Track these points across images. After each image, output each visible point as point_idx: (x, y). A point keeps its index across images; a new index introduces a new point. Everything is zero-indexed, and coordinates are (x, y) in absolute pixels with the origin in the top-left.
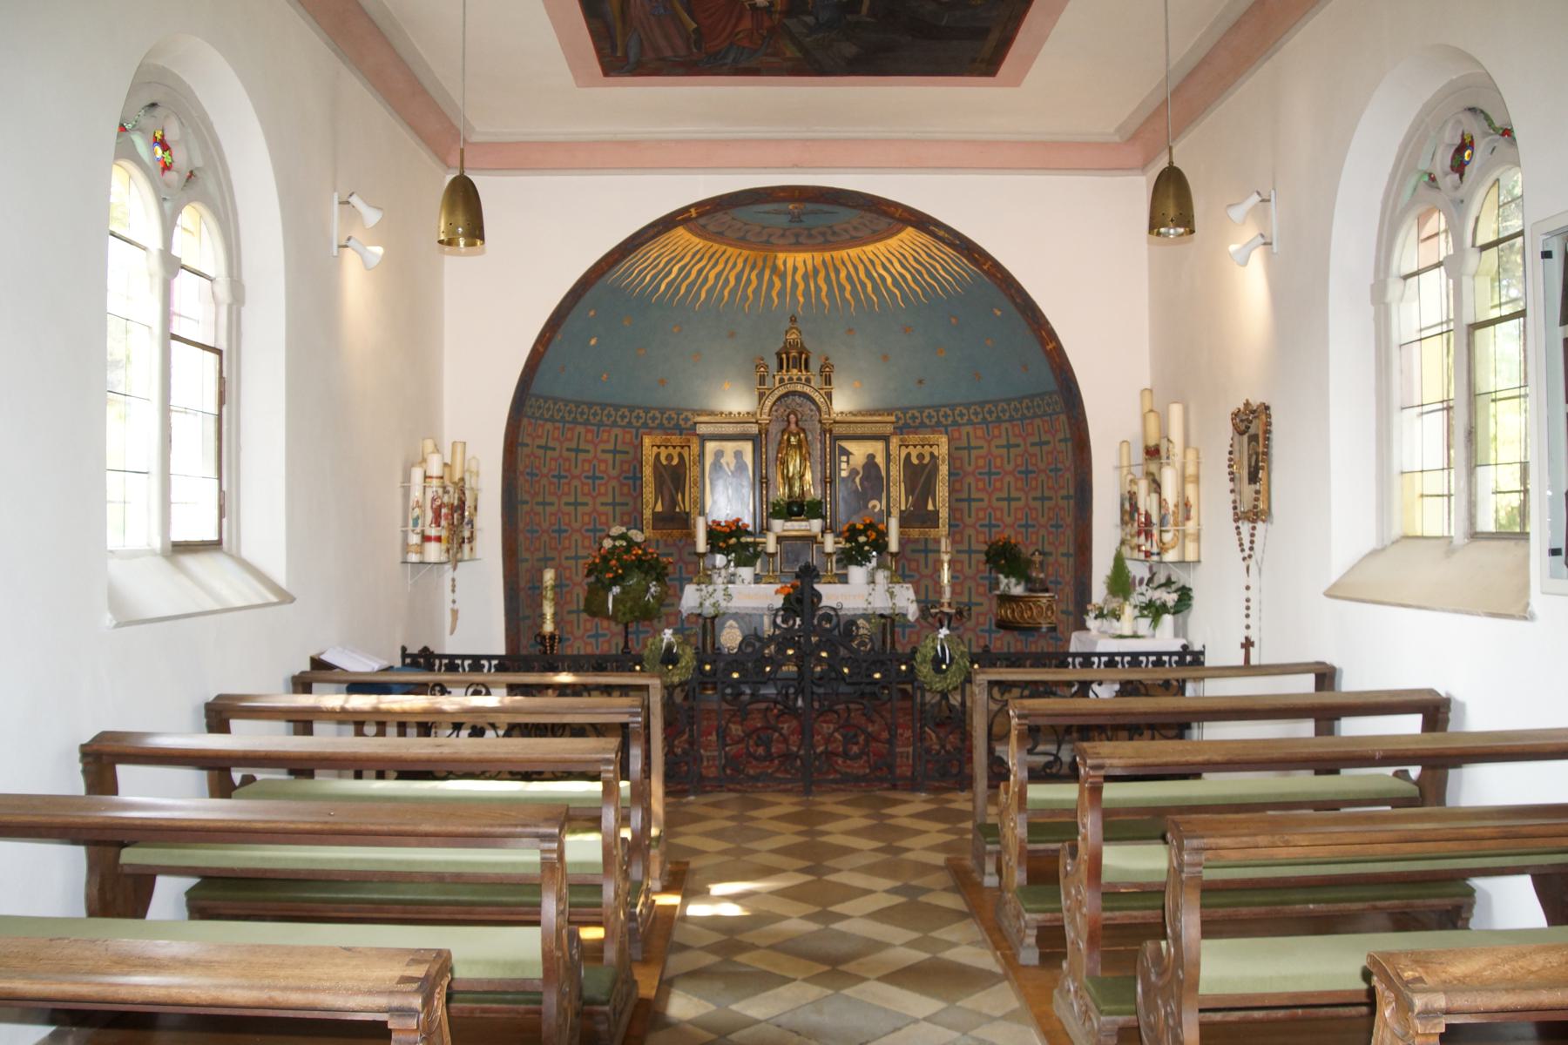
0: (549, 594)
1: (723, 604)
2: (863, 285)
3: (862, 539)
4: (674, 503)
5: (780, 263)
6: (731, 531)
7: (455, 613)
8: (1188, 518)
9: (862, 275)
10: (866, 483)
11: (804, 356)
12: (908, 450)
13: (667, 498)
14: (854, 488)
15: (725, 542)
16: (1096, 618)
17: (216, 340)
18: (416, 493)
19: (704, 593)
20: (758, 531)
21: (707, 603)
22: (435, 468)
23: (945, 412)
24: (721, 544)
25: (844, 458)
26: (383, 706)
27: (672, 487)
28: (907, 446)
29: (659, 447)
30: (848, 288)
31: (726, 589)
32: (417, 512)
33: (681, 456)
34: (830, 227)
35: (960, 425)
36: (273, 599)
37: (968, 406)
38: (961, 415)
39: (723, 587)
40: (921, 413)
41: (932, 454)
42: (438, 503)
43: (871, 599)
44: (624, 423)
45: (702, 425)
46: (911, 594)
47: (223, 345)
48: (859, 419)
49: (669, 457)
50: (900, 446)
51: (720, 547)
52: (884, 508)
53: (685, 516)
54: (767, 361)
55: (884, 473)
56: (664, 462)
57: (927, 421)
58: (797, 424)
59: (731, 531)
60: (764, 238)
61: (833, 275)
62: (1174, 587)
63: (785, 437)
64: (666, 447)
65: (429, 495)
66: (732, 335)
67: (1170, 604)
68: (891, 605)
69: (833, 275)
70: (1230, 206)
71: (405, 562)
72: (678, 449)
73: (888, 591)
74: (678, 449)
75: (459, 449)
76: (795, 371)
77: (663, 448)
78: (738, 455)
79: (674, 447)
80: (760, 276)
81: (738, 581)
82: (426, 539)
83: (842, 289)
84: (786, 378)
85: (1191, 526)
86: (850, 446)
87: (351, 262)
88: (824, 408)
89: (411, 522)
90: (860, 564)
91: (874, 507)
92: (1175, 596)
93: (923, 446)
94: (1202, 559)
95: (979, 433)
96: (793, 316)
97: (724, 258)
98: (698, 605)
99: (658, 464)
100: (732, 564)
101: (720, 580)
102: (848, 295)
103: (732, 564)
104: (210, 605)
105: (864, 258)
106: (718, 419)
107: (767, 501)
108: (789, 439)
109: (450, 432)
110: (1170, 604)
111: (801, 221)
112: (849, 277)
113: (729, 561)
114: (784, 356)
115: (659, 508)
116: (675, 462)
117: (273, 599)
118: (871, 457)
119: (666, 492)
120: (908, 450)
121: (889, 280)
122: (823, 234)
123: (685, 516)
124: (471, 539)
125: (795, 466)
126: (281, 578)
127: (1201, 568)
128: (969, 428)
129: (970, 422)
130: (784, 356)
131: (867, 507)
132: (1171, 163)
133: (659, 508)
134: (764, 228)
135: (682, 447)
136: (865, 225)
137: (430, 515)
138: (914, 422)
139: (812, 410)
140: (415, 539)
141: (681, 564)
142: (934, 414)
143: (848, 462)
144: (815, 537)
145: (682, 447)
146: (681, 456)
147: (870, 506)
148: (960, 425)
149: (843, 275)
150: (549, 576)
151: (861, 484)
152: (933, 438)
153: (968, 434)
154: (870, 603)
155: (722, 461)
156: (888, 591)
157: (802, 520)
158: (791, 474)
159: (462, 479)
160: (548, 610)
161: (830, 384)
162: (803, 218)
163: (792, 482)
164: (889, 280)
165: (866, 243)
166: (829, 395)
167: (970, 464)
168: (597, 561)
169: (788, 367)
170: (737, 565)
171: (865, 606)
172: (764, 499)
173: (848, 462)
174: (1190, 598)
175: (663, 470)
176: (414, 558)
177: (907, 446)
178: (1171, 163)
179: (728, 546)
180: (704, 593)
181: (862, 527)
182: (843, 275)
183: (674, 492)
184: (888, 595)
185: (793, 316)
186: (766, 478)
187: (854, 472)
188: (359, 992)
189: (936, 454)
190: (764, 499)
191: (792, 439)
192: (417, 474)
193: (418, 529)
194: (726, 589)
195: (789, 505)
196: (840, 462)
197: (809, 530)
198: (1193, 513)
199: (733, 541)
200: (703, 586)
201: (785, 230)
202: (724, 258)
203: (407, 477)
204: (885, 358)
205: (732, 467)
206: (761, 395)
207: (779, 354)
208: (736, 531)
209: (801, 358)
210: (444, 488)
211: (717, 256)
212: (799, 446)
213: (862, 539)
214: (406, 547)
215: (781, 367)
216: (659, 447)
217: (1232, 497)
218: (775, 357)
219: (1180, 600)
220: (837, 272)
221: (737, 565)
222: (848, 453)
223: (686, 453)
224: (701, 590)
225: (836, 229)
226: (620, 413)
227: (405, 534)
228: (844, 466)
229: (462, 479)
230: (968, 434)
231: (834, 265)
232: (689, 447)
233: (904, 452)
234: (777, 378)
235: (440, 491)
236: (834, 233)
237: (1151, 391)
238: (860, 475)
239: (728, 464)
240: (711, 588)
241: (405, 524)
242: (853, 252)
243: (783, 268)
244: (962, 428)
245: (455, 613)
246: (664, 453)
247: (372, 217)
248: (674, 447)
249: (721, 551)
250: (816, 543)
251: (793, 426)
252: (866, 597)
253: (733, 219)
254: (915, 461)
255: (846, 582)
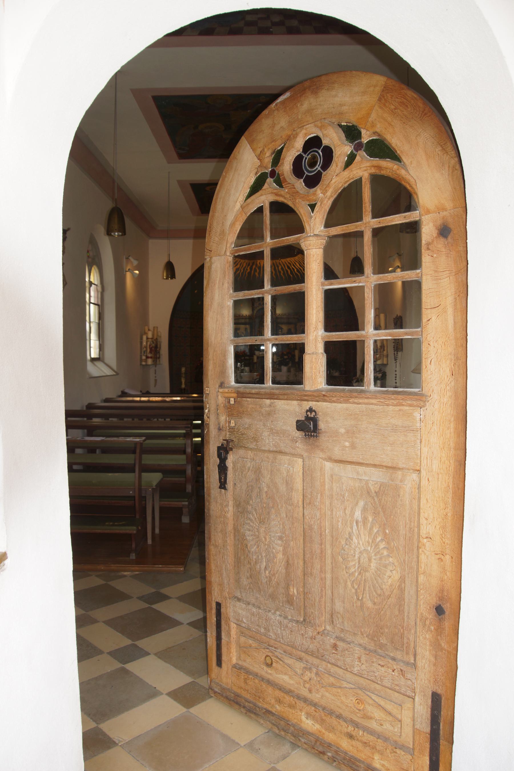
0: (183, 375)
2: (287, 271)
5: (258, 263)
7: (156, 380)
8: (384, 350)
9: (287, 268)
16: (356, 382)
17: (98, 302)
18: (144, 343)
22: (150, 335)
25: (280, 330)
26: (151, 400)
30: (282, 272)
32: (145, 349)
36: (115, 374)
42: (151, 346)
47: (100, 303)
61: (277, 268)
62: (382, 372)
65: (148, 344)
67: (379, 377)
69: (277, 268)
70: (390, 257)
71: (141, 365)
75: (156, 329)
78: (246, 329)
80: (251, 269)
81: (244, 371)
82: (147, 357)
83: (280, 272)
85: (385, 352)
87: (128, 275)
89: (143, 352)
92: (381, 375)
94: (389, 363)
97: (240, 263)
102: (282, 274)
104: (104, 375)
105: (287, 262)
109: (152, 323)
110: (379, 377)
112: (282, 268)
117: (115, 374)
121: (295, 270)
124: (159, 358)
126: (115, 368)
127: (388, 366)
132: (357, 255)
137: (148, 350)
140: (144, 358)
149: (280, 268)
150: (183, 370)
159: (157, 339)
160: (183, 381)
164: (295, 270)
165: (287, 257)
168: (199, 364)
170: (244, 366)
174: (386, 375)
176: (144, 363)
178: (357, 255)
182: (280, 268)
192: (145, 338)
193: (145, 354)
198: (385, 348)
199: (243, 358)
202: (240, 263)
203: (141, 338)
210: (153, 341)
211: (238, 262)
213: (285, 357)
214: (141, 360)
217: (394, 344)
219: (382, 376)
220: (278, 267)
221: (244, 366)
222: (282, 329)
227: (141, 356)
229: (157, 339)
231: (277, 265)
235: (152, 342)
237: (379, 309)
241: (141, 353)
242: (283, 260)
243: (259, 265)
245: (156, 380)
247: (135, 263)
255: (281, 371)
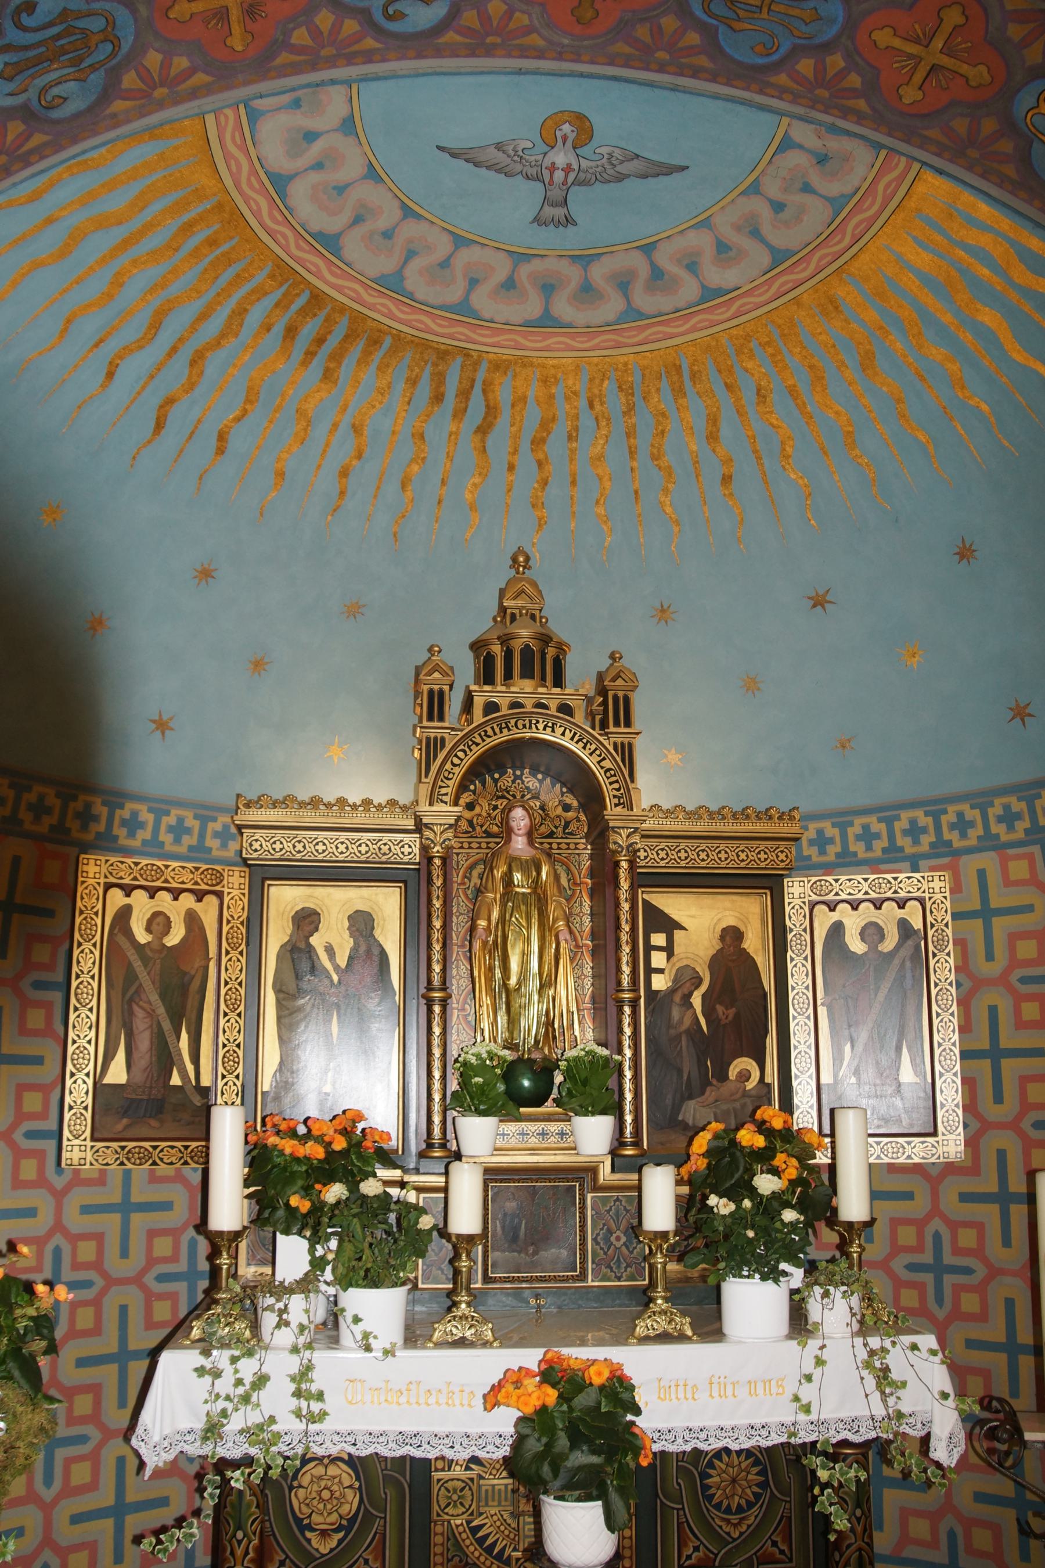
1: (288, 1424)
3: (766, 1184)
4: (166, 1059)
6: (330, 1154)
10: (720, 1009)
11: (551, 652)
12: (835, 916)
13: (144, 1042)
14: (687, 1022)
15: (307, 1191)
19: (225, 1385)
20: (413, 1148)
21: (235, 1423)
23: (913, 822)
24: (294, 1201)
25: (659, 939)
27: (161, 1010)
28: (832, 907)
29: (128, 891)
31: (305, 1373)
33: (192, 920)
34: (648, 249)
35: (957, 853)
37: (981, 799)
38: (962, 825)
39: (293, 1364)
40: (843, 827)
41: (904, 925)
43: (807, 1392)
44: (43, 828)
45: (259, 834)
46: (939, 1377)
48: (701, 827)
49: (159, 922)
50: (813, 906)
51: (292, 1211)
52: (772, 1076)
53: (197, 1101)
54: (448, 657)
55: (768, 983)
56: (142, 937)
57: (858, 848)
58: (530, 835)
59: (330, 1154)
60: (454, 294)
63: (498, 874)
64: (152, 893)
66: (354, 610)
68: (879, 1411)
72: (187, 901)
73: (868, 1365)
74: (187, 901)
76: (527, 685)
77: (139, 896)
79: (176, 894)
81: (348, 1334)
84: (504, 702)
86: (673, 904)
88: (608, 791)
90: (773, 1275)
91: (745, 1076)
93: (878, 905)
95: (1019, 869)
96: (520, 551)
98: (199, 1425)
99: (122, 940)
100: (328, 1275)
101: (285, 1337)
103: (328, 1275)
106: (309, 817)
107: (444, 1055)
108: (508, 881)
111: (569, 221)
113: (318, 1264)
114: (497, 649)
115: (117, 1074)
116: (175, 937)
118: (732, 936)
119: (141, 1022)
120: (835, 916)
122: (624, 283)
123: (197, 1101)
125: (525, 956)
128: (988, 861)
129: (989, 843)
130: (497, 649)
131: (723, 1077)
133: (117, 1074)
134: (460, 241)
135: (200, 896)
136: (755, 233)
138: (822, 852)
139: (567, 808)
141: (149, 1279)
142: (881, 828)
143: (669, 950)
144: (592, 1170)
145: (200, 896)
146: (192, 920)
147: (733, 1072)
148: (957, 853)
151: (708, 1010)
152: (908, 882)
153: (982, 874)
154: (807, 1409)
155: (316, 941)
156: (868, 1365)
157: (549, 1118)
158: (513, 981)
161: (628, 724)
162: (577, 194)
163: (516, 1003)
166: (627, 753)
167: (990, 956)
169: (508, 676)
170: (345, 1281)
171: (789, 1419)
172: (437, 1052)
173: (669, 950)
175: (137, 965)
177: (832, 907)
179: (318, 1207)
180: (225, 1385)
181: (760, 1142)
183: (167, 1025)
184: (871, 1382)
185: (520, 551)
186: (430, 1003)
187: (686, 979)
188: (444, 970)
189: (917, 924)
190: (437, 1052)
191: (517, 877)
194: (305, 1373)
195: (510, 1072)
196: (649, 948)
197: (501, 1121)
200: (221, 1357)
201: (520, 258)
204: (751, 685)
205: (342, 961)
206: (432, 747)
207: (477, 646)
208: (345, 1153)
209: (543, 655)
212: (539, 899)
213: (766, 1184)
215: (487, 678)
216: (128, 891)
218: (470, 655)
222: (669, 926)
223: (208, 911)
224: (217, 1374)
225: (663, 258)
226: (31, 797)
228: (658, 959)
230: (982, 874)
232: (219, 895)
233: (824, 920)
234: (479, 702)
236: (657, 273)
238: (704, 988)
239: (330, 950)
240: (248, 1368)
244: (964, 859)
246: (142, 905)
248: (176, 894)
249: (294, 1223)
250: (597, 1188)
251: (519, 844)
252: (791, 1388)
253: (372, 174)
254: (856, 946)
